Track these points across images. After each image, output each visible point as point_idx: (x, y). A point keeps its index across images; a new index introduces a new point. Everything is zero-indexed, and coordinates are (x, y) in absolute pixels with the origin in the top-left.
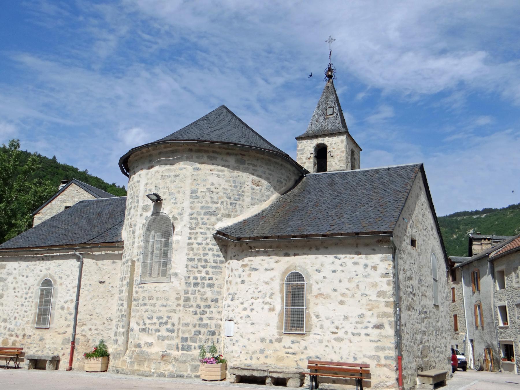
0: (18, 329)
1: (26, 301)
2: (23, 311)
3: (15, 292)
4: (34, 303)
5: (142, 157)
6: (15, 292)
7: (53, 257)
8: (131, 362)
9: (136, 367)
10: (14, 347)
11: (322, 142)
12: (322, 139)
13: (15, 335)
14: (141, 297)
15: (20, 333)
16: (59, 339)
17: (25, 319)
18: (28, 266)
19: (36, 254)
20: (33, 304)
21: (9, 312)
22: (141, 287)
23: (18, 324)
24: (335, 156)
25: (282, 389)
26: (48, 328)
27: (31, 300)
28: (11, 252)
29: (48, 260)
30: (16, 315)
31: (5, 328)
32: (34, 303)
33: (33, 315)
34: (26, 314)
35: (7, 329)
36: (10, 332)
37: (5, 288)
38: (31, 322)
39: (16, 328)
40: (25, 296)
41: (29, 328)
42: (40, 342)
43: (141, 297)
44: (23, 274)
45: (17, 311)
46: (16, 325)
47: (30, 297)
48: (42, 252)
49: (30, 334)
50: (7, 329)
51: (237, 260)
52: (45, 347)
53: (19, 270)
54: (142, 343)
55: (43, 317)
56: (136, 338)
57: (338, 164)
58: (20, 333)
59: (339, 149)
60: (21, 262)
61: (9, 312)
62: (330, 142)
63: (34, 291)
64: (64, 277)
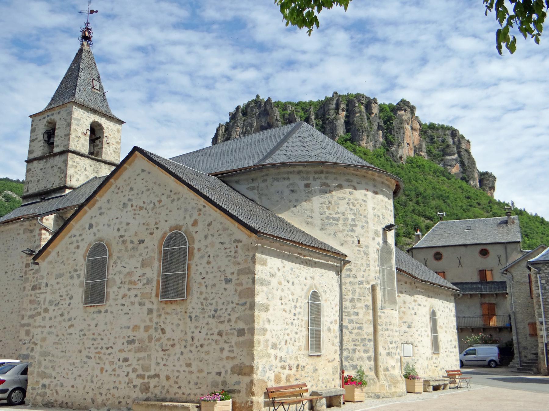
0: (291, 358)
1: (296, 318)
2: (293, 332)
3: (282, 304)
4: (304, 322)
5: (365, 176)
6: (282, 304)
7: (315, 263)
8: (389, 386)
9: (394, 390)
10: (288, 384)
11: (99, 121)
12: (100, 118)
13: (287, 368)
14: (384, 322)
15: (293, 363)
16: (330, 368)
17: (297, 344)
18: (292, 269)
19: (299, 254)
20: (303, 323)
21: (279, 332)
22: (383, 312)
23: (290, 351)
24: (110, 144)
25: (21, 410)
26: (319, 356)
27: (300, 317)
28: (287, 245)
29: (311, 266)
30: (287, 338)
31: (276, 357)
32: (304, 322)
33: (304, 338)
34: (297, 336)
35: (278, 358)
36: (283, 363)
37: (270, 296)
38: (303, 347)
39: (288, 356)
40: (293, 311)
41: (302, 356)
42: (314, 375)
43: (384, 322)
44: (289, 279)
45: (287, 332)
46: (288, 352)
47: (300, 313)
48: (320, 256)
49: (304, 364)
50: (278, 358)
51: (409, 295)
52: (319, 380)
53: (284, 272)
54: (389, 366)
55: (315, 342)
56: (385, 362)
57: (113, 155)
58: (293, 363)
59: (114, 138)
60: (285, 262)
61: (279, 332)
62: (106, 126)
63: (302, 305)
64: (328, 292)
